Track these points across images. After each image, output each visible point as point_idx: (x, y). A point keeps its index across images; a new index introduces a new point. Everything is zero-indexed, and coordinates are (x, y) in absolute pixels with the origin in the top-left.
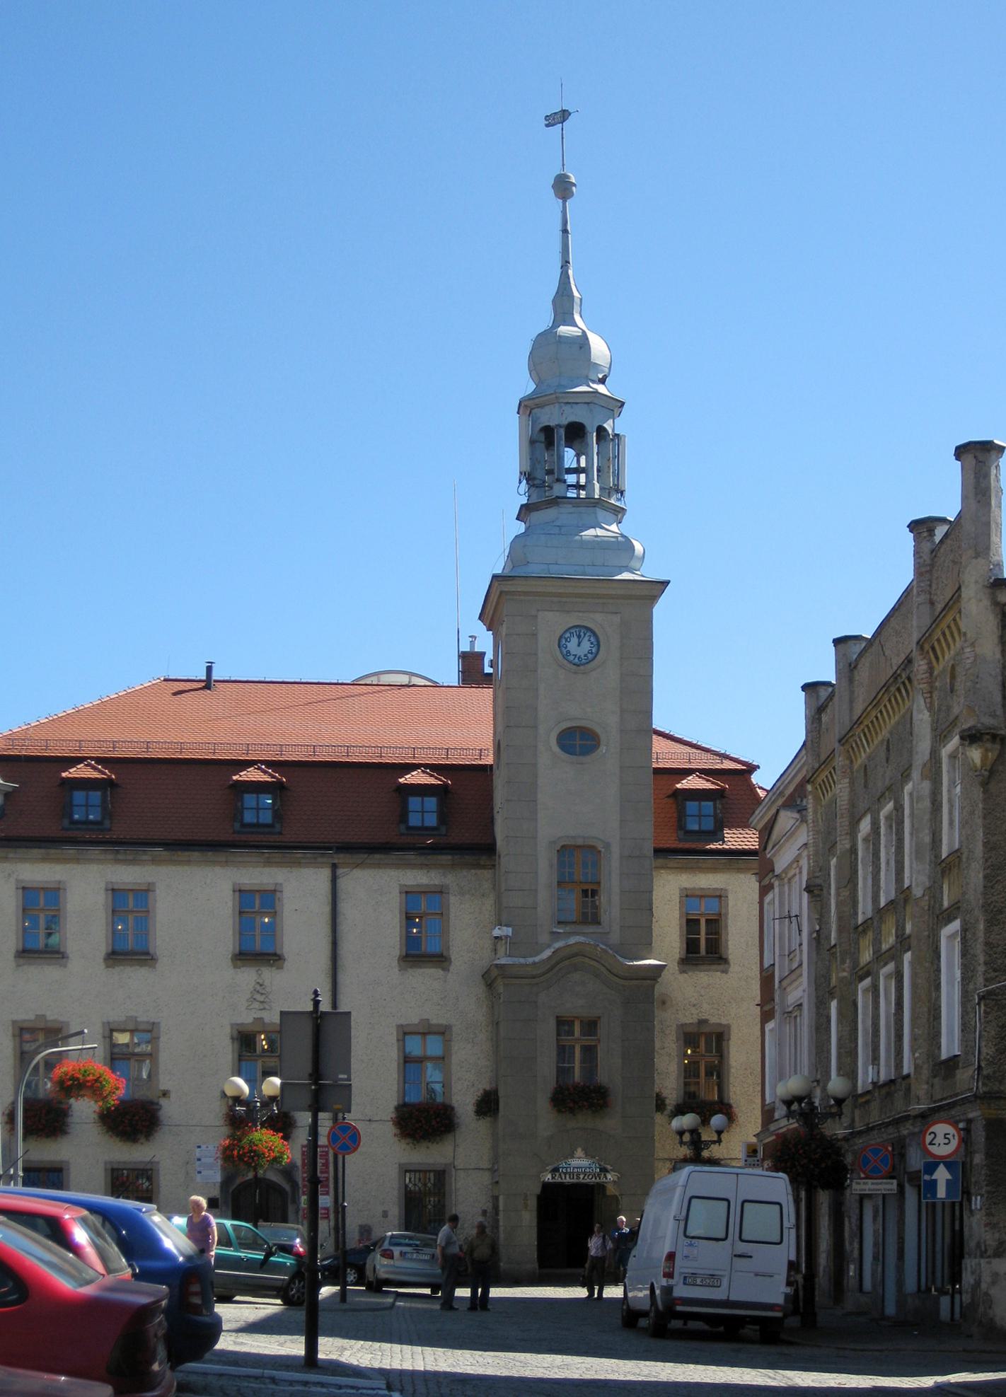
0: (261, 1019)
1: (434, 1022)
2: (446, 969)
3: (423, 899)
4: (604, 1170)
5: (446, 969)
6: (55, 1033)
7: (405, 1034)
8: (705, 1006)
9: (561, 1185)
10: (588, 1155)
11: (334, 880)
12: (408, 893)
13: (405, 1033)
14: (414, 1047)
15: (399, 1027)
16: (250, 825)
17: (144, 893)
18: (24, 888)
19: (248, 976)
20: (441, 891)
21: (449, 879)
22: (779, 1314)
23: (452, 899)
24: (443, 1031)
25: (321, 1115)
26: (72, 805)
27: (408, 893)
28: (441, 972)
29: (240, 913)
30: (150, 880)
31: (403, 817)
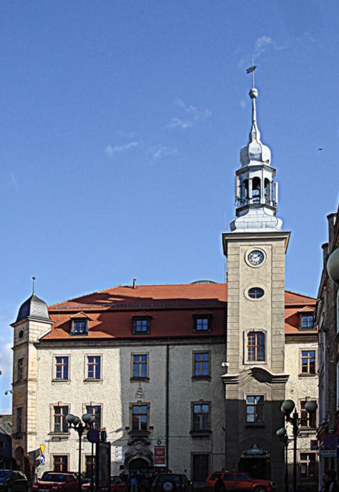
0: (141, 401)
1: (205, 400)
2: (210, 381)
3: (201, 356)
4: (265, 453)
5: (210, 381)
6: (66, 408)
7: (194, 405)
8: (309, 391)
9: (248, 459)
10: (258, 448)
11: (168, 350)
12: (195, 353)
13: (193, 404)
14: (197, 409)
15: (192, 402)
16: (199, 330)
17: (145, 356)
18: (134, 355)
19: (136, 385)
20: (208, 352)
21: (211, 348)
22: (95, 444)
23: (212, 356)
24: (208, 403)
25: (292, 461)
26: (202, 319)
27: (195, 353)
28: (207, 382)
29: (134, 363)
30: (191, 353)
31: (195, 327)
